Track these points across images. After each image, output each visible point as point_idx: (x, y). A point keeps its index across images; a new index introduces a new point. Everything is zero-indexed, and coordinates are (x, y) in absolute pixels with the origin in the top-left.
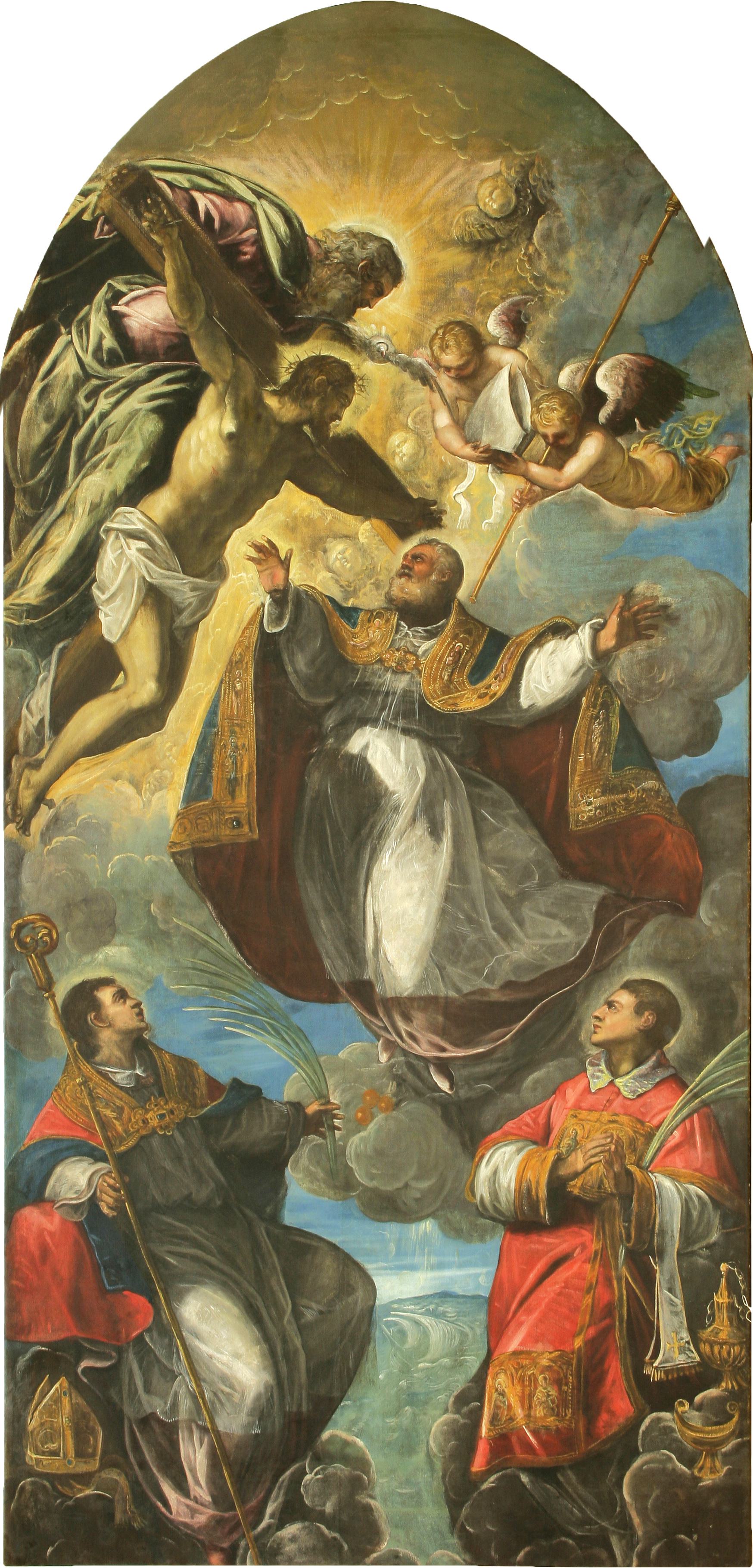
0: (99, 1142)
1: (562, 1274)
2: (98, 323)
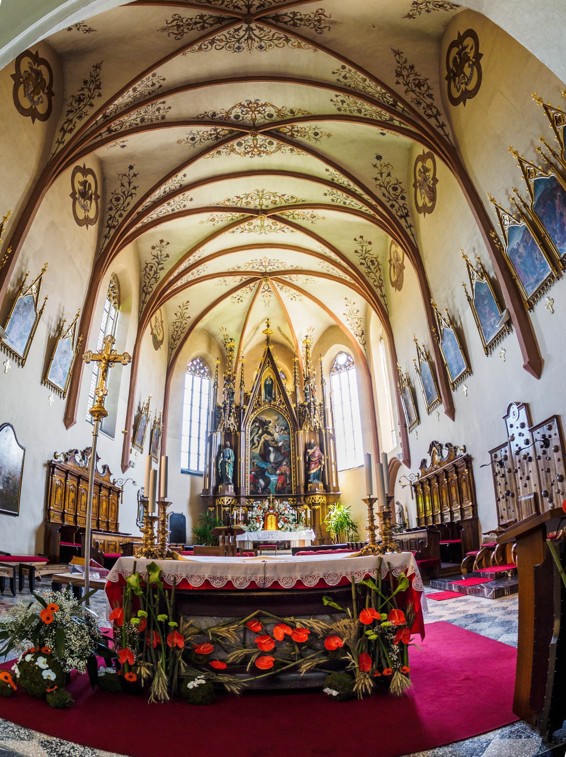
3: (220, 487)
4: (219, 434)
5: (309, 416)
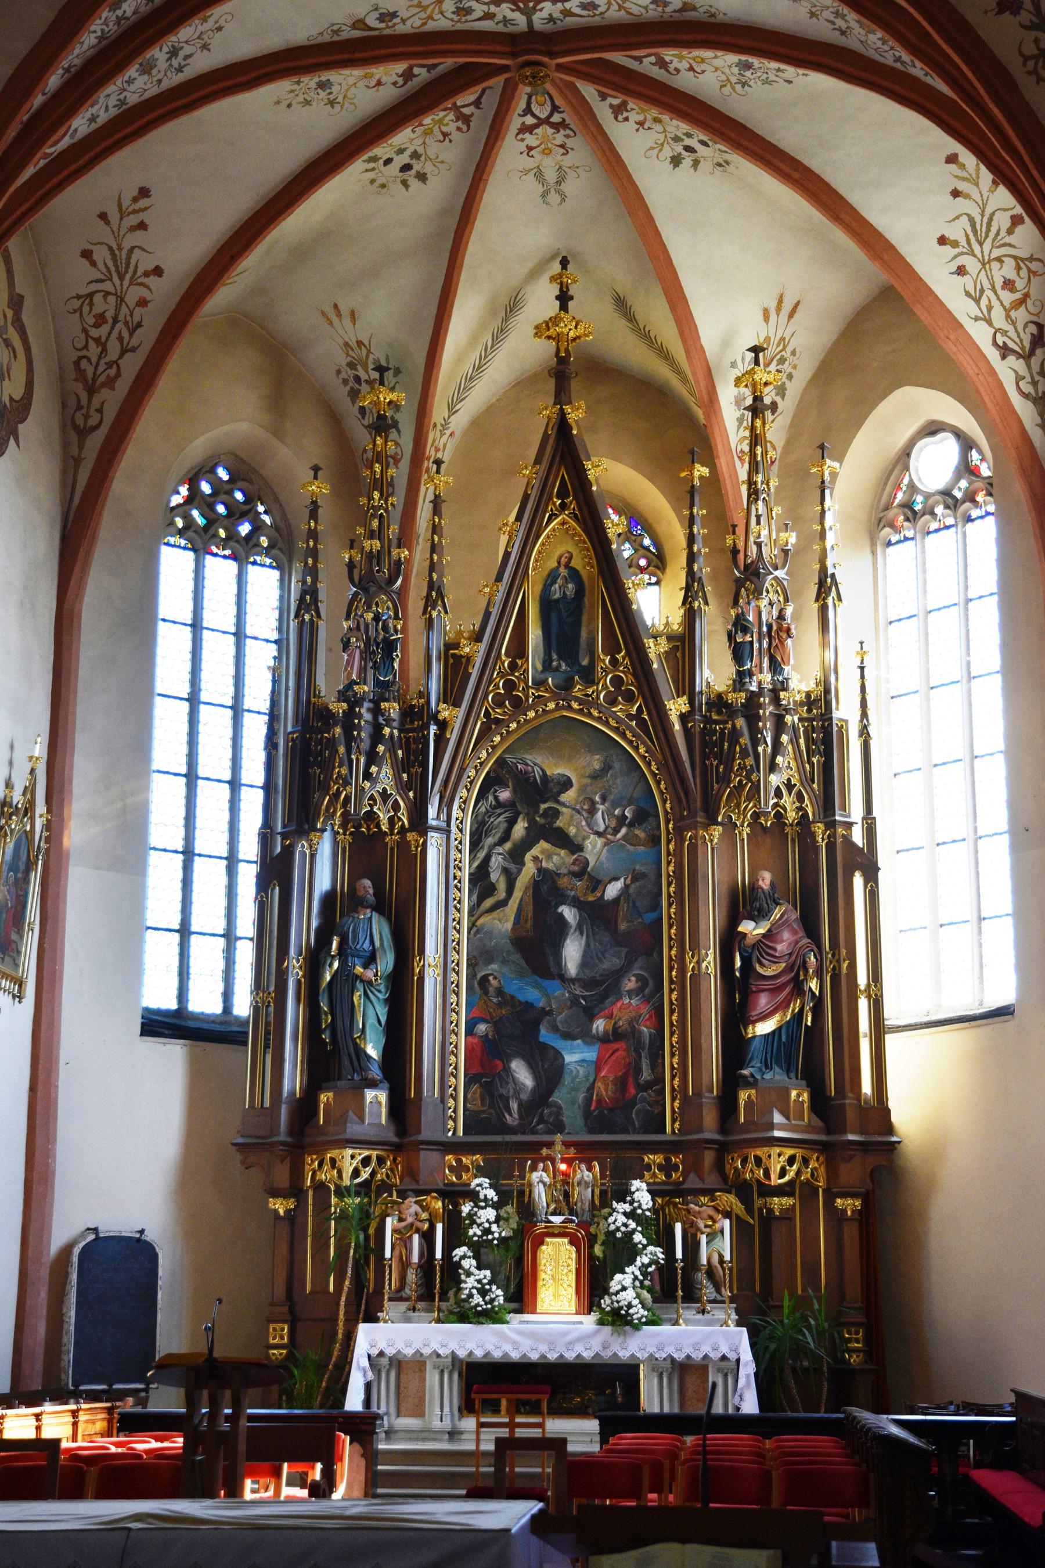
0: (488, 1018)
1: (616, 1054)
2: (491, 798)
3: (325, 1097)
4: (325, 847)
5: (750, 761)
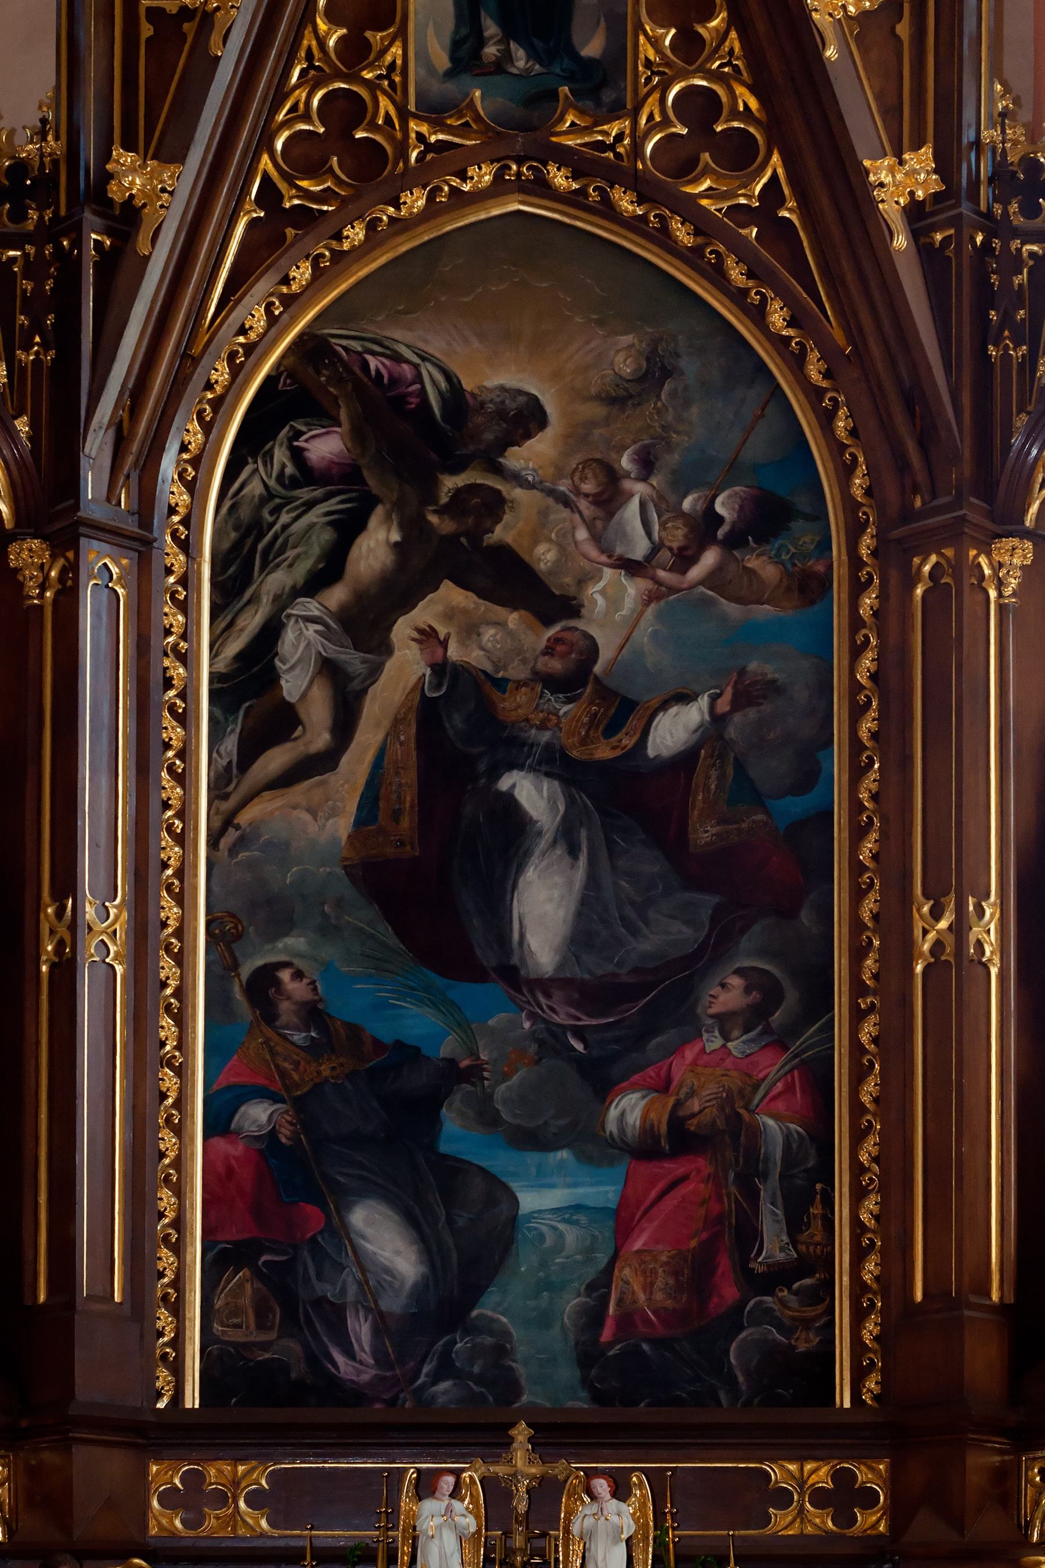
2: (280, 455)
